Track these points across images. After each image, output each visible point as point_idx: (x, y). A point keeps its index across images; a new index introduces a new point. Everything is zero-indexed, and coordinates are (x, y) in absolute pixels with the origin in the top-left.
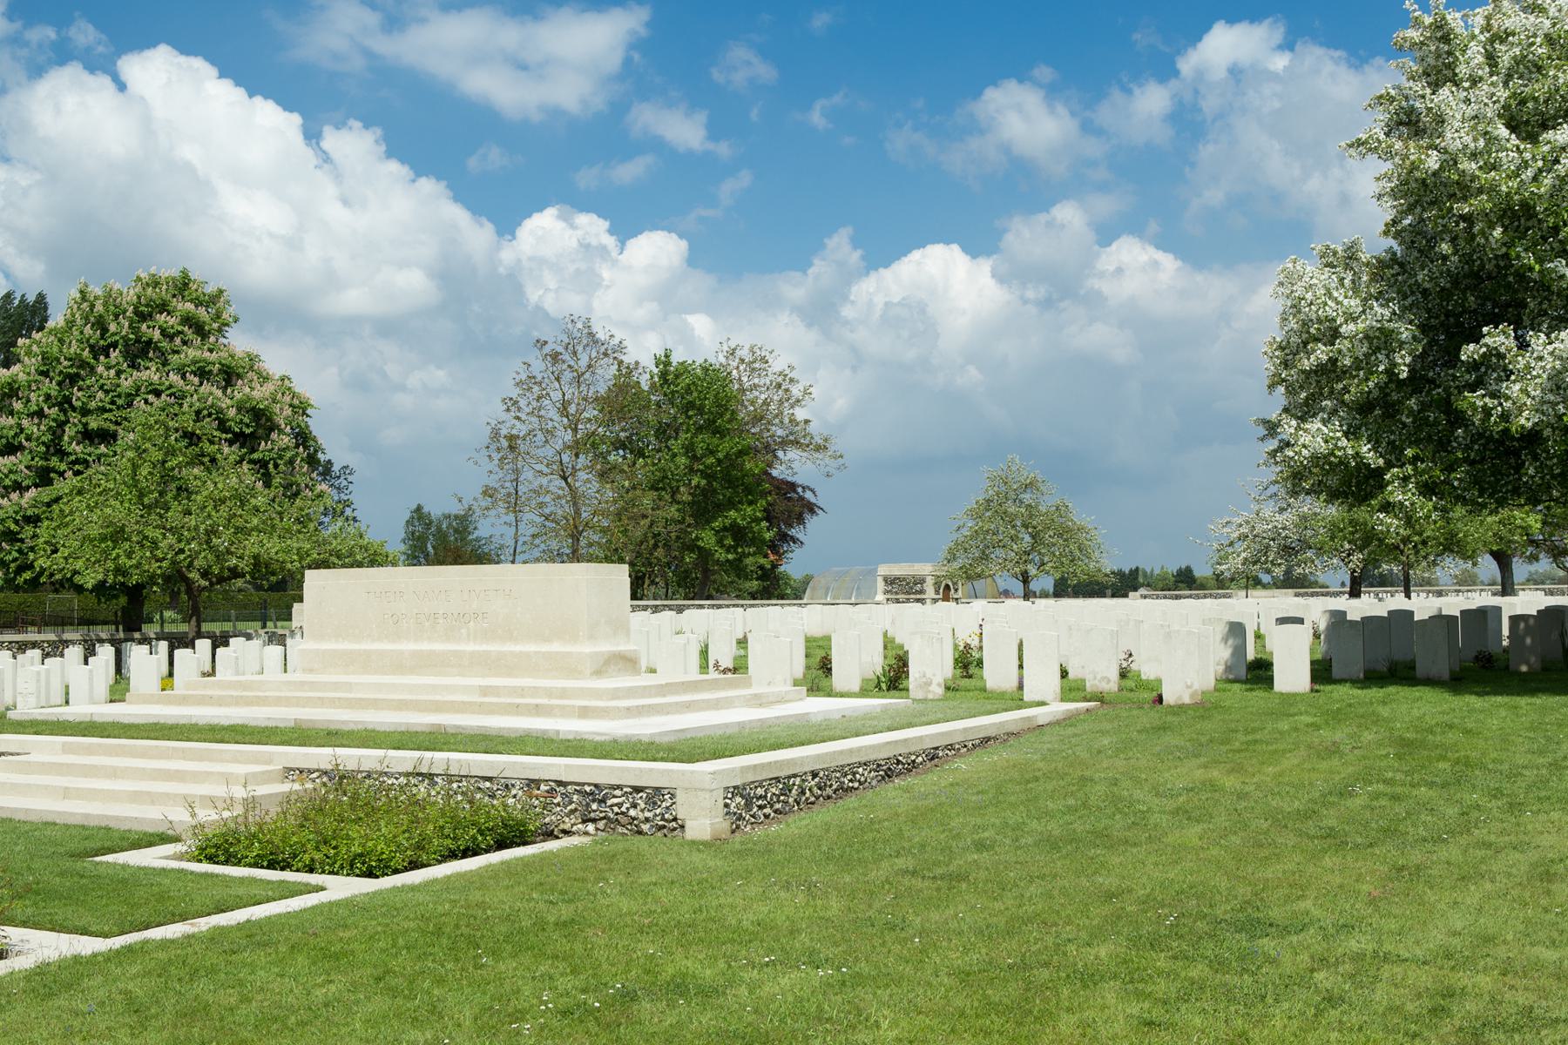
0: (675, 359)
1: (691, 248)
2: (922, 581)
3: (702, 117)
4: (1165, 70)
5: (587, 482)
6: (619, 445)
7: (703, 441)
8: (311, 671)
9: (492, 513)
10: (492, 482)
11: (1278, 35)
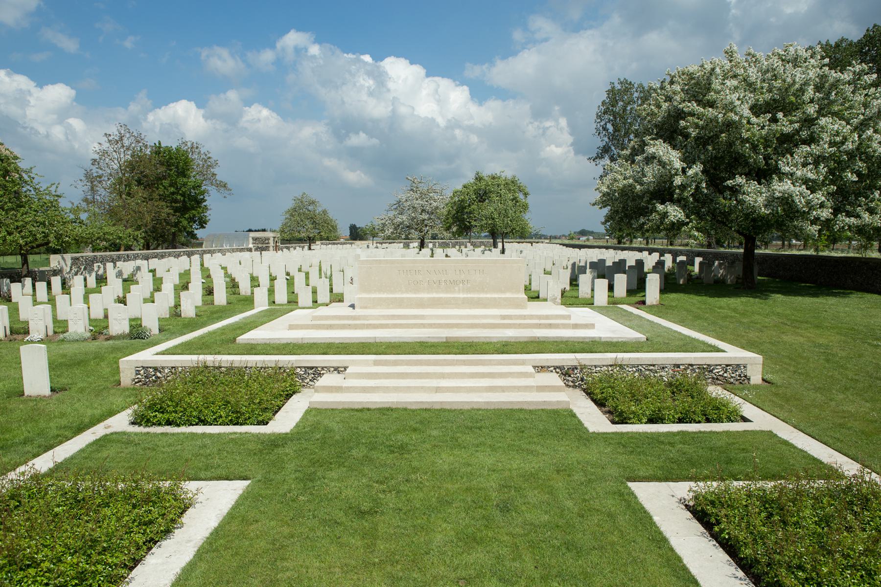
4: (273, 46)
8: (366, 308)
11: (312, 39)
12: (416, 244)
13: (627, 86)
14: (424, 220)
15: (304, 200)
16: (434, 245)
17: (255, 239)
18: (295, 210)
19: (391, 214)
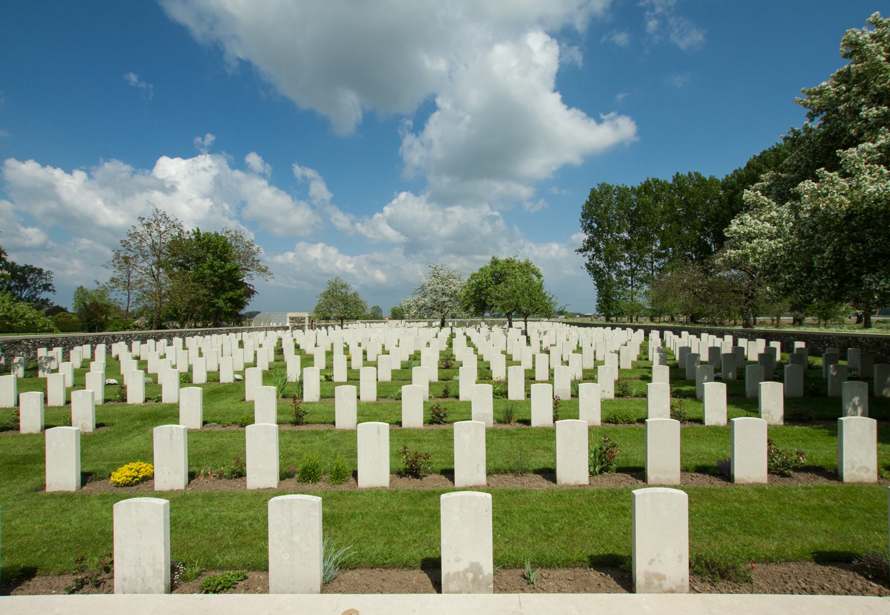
0: (201, 232)
1: (878, 421)
2: (304, 319)
3: (332, 195)
5: (163, 276)
6: (177, 265)
7: (217, 263)
9: (116, 289)
10: (116, 276)
12: (438, 323)
13: (606, 189)
14: (444, 302)
15: (338, 284)
16: (453, 323)
17: (292, 319)
18: (329, 292)
19: (416, 298)
